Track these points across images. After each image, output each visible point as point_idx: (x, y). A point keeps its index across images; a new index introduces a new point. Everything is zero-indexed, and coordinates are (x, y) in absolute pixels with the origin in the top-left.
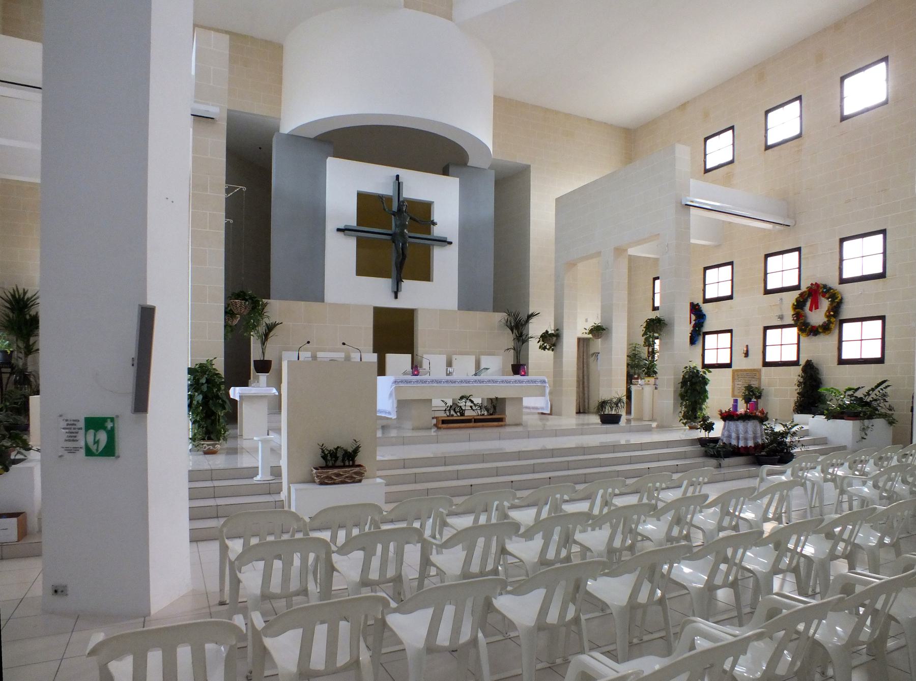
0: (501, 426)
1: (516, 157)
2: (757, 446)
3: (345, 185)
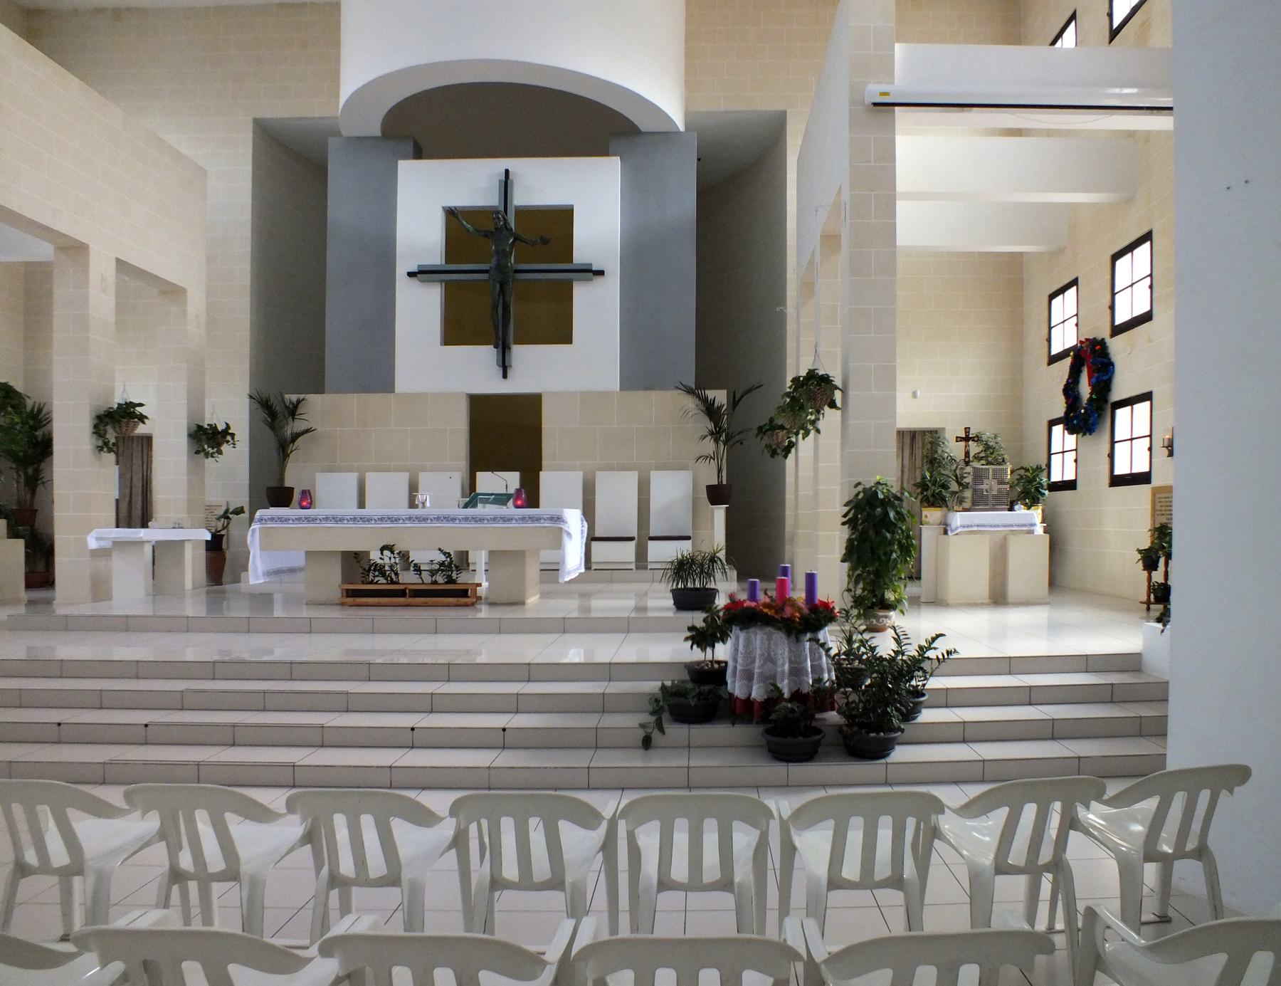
0: (466, 605)
1: (742, 97)
2: (774, 698)
3: (425, 200)
